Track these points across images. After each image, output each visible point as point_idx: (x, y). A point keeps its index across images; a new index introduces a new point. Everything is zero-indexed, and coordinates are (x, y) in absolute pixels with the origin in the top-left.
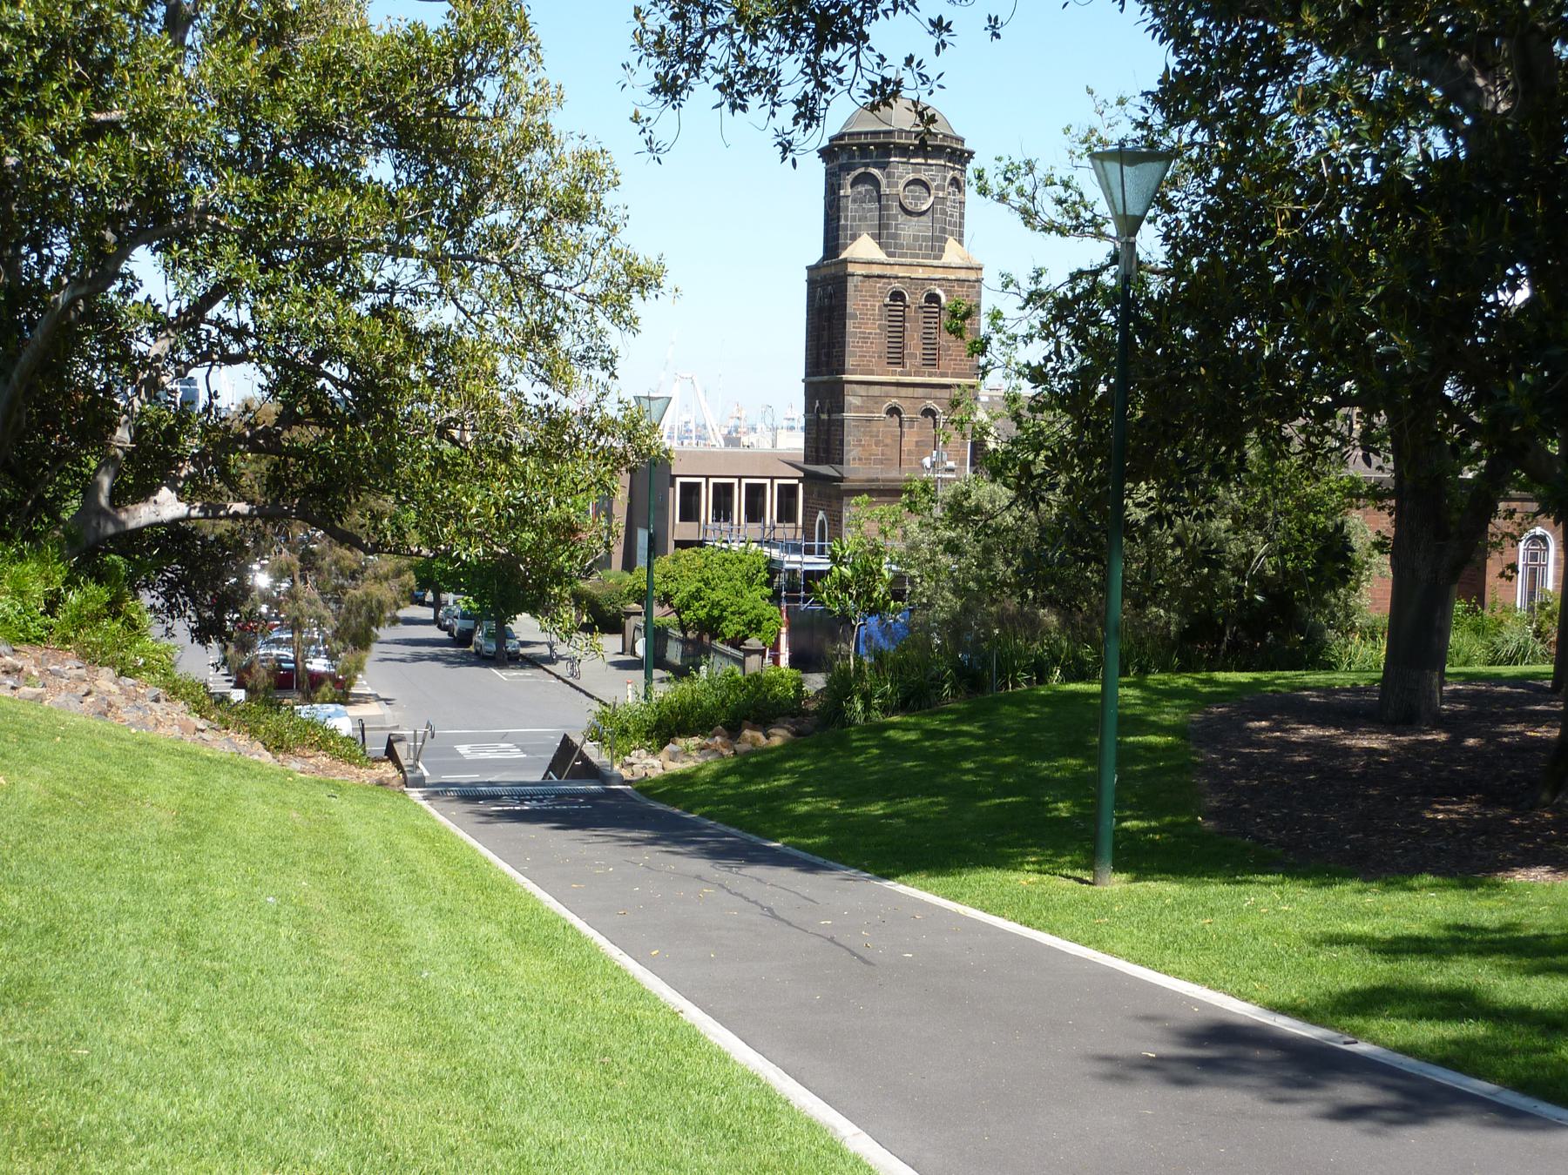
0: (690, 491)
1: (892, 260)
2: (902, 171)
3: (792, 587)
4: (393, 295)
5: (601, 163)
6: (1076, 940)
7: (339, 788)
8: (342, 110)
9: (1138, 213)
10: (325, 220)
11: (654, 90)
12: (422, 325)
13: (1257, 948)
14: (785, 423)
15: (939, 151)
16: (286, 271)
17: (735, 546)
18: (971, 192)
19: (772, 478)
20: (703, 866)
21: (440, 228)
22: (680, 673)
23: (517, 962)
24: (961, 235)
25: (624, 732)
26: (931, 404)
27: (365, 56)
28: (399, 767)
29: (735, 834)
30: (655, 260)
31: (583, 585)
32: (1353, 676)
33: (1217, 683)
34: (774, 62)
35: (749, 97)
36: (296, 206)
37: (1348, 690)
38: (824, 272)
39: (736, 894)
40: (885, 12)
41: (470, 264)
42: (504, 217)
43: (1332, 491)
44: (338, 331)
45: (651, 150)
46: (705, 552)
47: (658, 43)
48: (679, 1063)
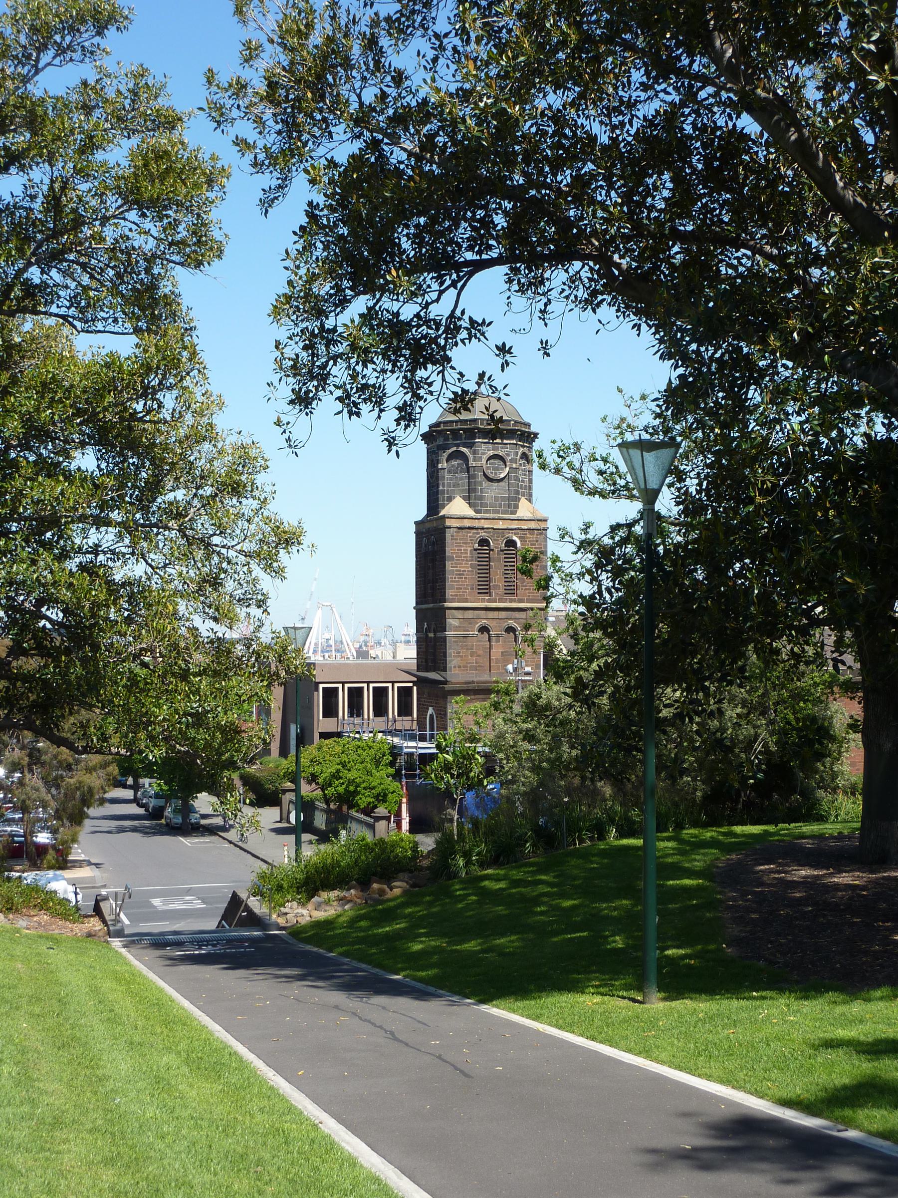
0: (330, 695)
1: (479, 516)
2: (485, 449)
3: (410, 766)
4: (97, 555)
5: (253, 453)
6: (629, 1051)
7: (56, 941)
8: (56, 417)
9: (656, 487)
10: (43, 501)
11: (292, 402)
12: (118, 577)
13: (770, 1053)
14: (403, 638)
15: (511, 434)
16: (15, 539)
17: (366, 736)
18: (535, 467)
19: (393, 683)
20: (338, 997)
21: (131, 504)
22: (324, 837)
23: (191, 1086)
24: (531, 495)
25: (280, 888)
26: (512, 623)
27: (73, 378)
28: (104, 921)
29: (365, 969)
30: (296, 524)
31: (253, 769)
32: (839, 826)
33: (735, 835)
34: (380, 380)
35: (361, 406)
36: (21, 491)
37: (835, 838)
38: (428, 525)
39: (365, 1020)
40: (462, 341)
41: (155, 530)
42: (180, 495)
43: (816, 685)
44: (55, 583)
45: (290, 446)
46: (343, 741)
47: (294, 367)
48: (316, 1169)
